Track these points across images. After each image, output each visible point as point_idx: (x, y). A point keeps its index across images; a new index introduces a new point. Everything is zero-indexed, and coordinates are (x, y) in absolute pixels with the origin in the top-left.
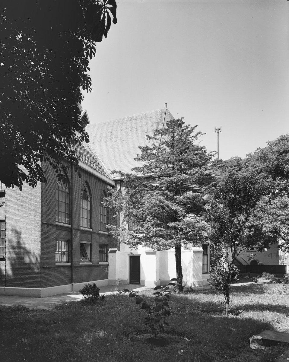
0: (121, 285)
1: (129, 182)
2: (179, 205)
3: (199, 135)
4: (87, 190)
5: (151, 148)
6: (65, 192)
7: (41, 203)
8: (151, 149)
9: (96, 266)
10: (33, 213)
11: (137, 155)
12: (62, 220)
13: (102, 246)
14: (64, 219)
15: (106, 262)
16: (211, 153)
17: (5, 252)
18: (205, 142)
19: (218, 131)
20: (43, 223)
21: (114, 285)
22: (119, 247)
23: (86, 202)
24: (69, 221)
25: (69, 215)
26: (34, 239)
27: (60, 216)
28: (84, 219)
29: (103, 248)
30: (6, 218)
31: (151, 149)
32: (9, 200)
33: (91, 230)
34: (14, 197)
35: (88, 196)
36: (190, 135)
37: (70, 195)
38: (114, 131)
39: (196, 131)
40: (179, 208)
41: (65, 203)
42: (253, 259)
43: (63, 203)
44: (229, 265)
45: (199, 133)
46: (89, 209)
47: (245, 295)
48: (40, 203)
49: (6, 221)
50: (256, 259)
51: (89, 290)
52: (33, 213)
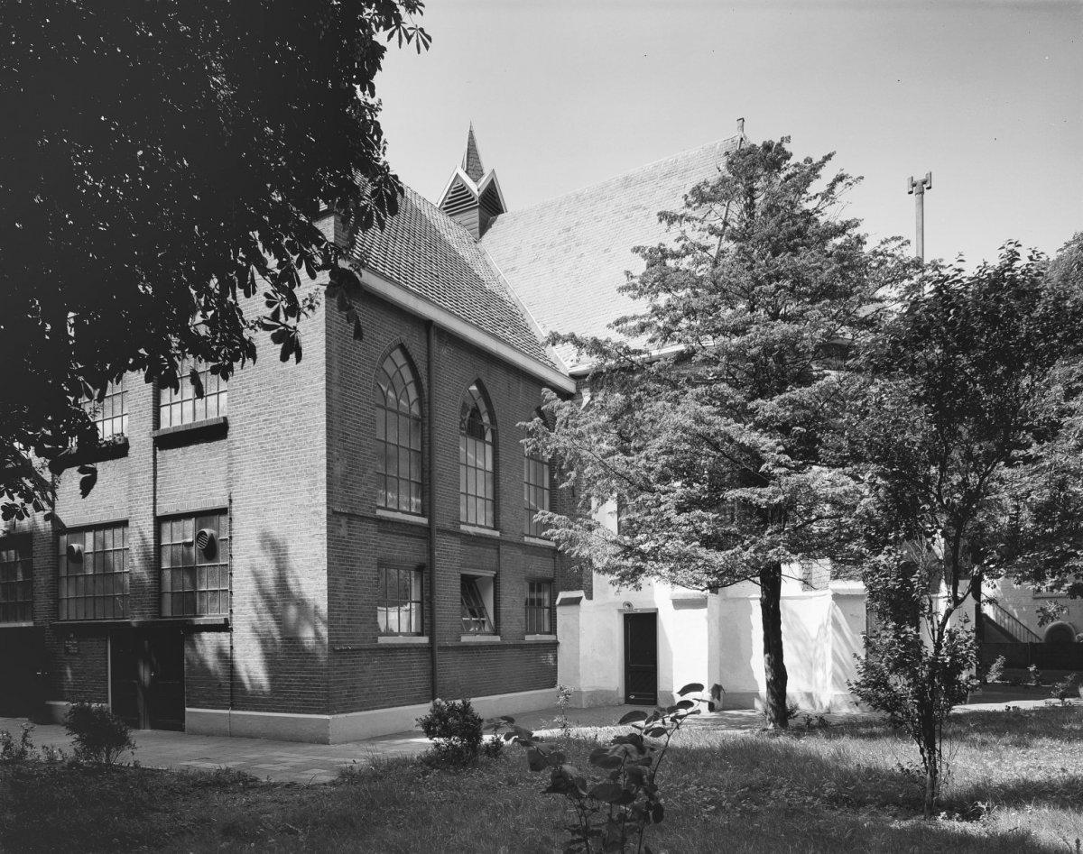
0: (596, 708)
1: (618, 374)
2: (766, 432)
3: (840, 186)
4: (483, 408)
5: (674, 250)
6: (408, 416)
7: (327, 448)
8: (676, 256)
9: (514, 646)
10: (305, 482)
11: (627, 273)
12: (403, 507)
13: (537, 584)
14: (404, 498)
15: (550, 633)
16: (882, 247)
17: (231, 607)
18: (873, 213)
19: (920, 187)
20: (335, 513)
21: (574, 706)
22: (591, 586)
23: (480, 444)
24: (423, 505)
25: (422, 489)
26: (308, 564)
27: (393, 492)
28: (471, 500)
29: (539, 591)
30: (231, 501)
31: (676, 256)
32: (238, 448)
33: (497, 534)
34: (252, 438)
35: (486, 427)
36: (808, 190)
37: (424, 423)
38: (577, 224)
39: (828, 174)
40: (767, 440)
41: (409, 450)
42: (1059, 622)
43: (478, 471)
44: (936, 626)
45: (841, 178)
46: (489, 467)
47: (1018, 745)
48: (325, 451)
49: (231, 511)
50: (1067, 623)
51: (446, 720)
52: (305, 482)
